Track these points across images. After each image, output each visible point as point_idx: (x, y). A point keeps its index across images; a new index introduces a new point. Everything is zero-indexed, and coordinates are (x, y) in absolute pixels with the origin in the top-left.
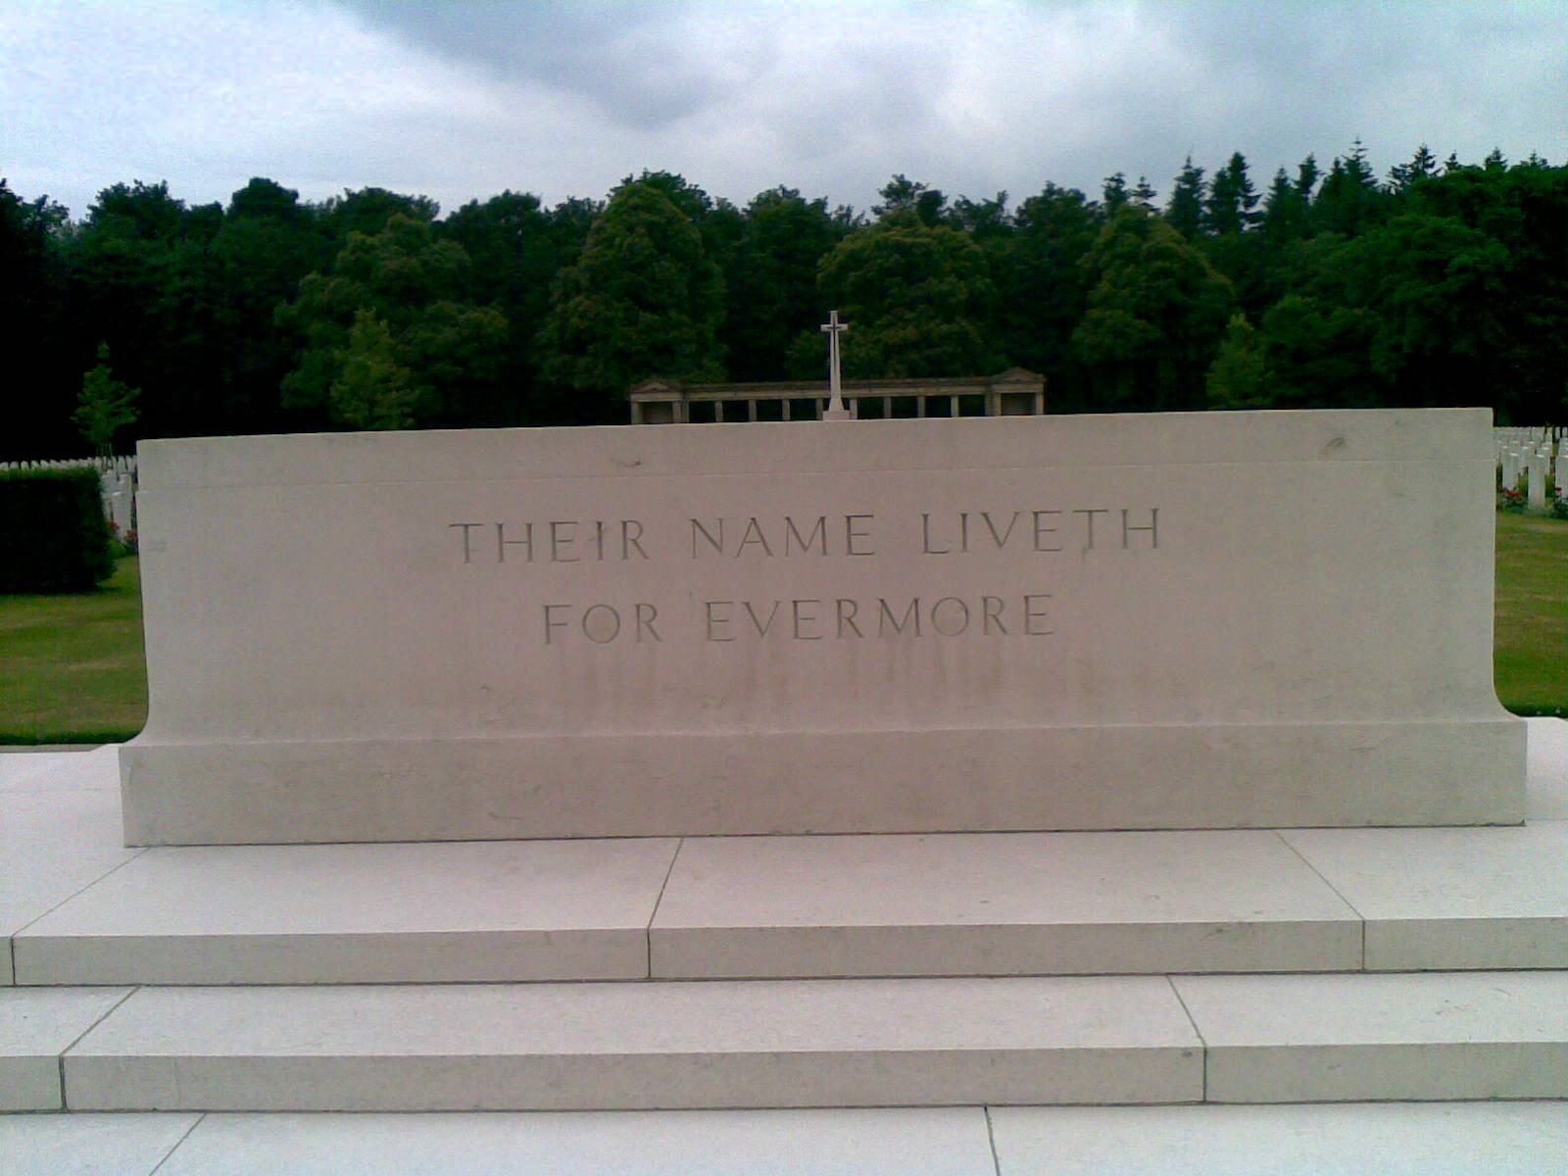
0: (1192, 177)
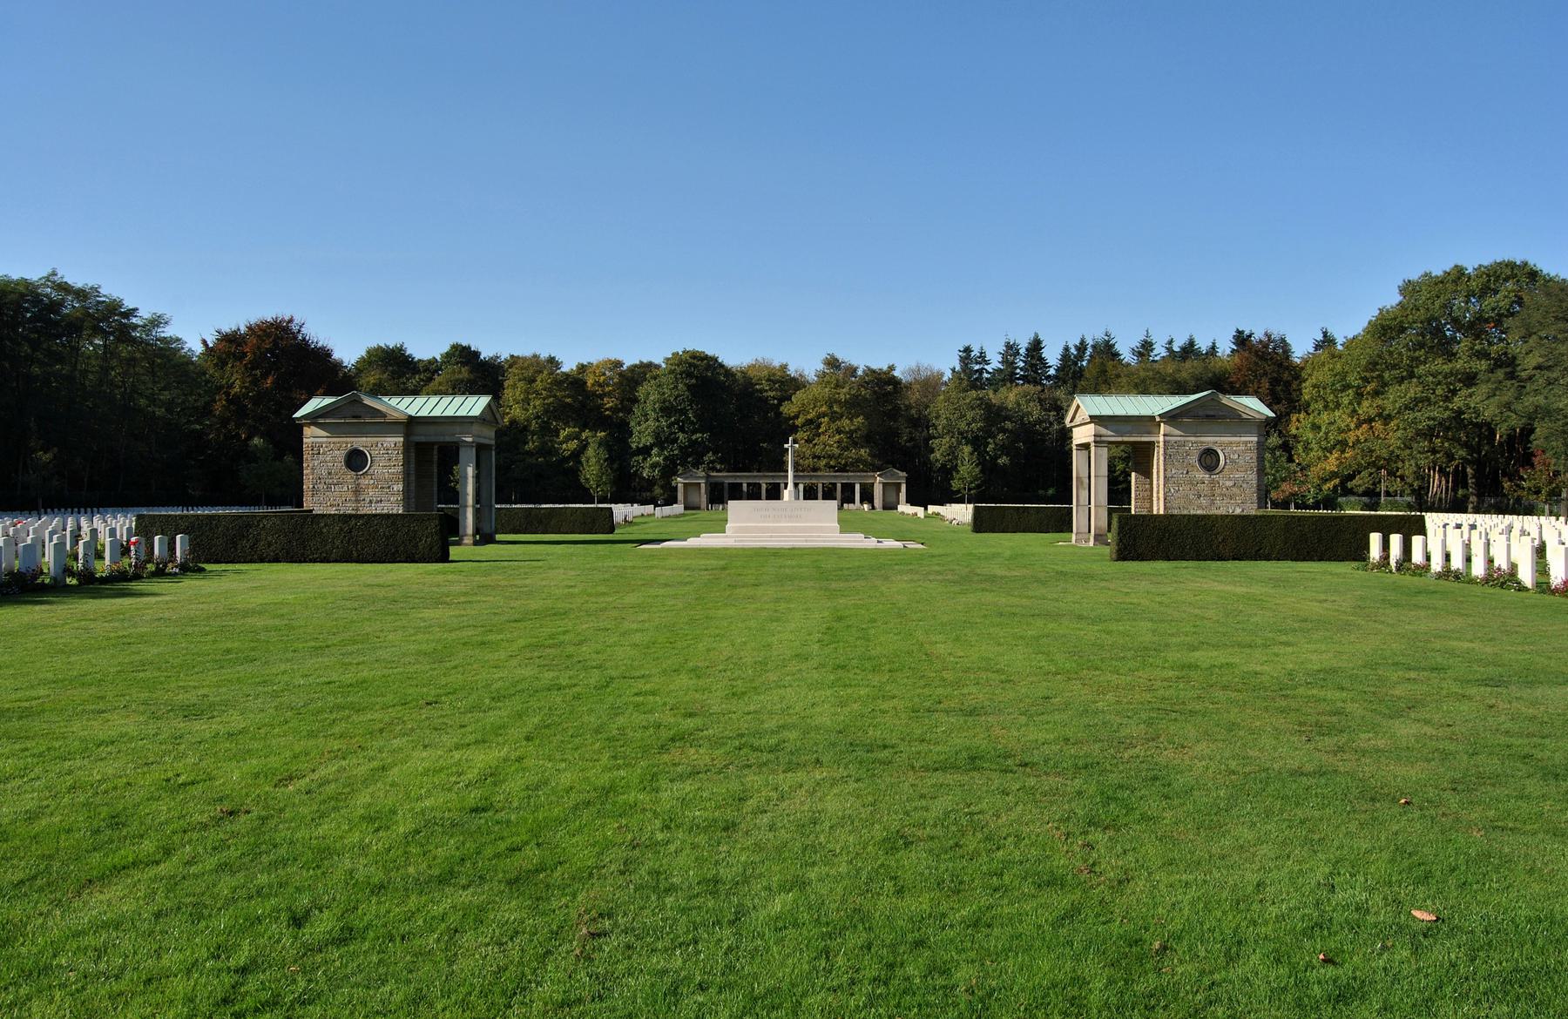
0: (1011, 349)
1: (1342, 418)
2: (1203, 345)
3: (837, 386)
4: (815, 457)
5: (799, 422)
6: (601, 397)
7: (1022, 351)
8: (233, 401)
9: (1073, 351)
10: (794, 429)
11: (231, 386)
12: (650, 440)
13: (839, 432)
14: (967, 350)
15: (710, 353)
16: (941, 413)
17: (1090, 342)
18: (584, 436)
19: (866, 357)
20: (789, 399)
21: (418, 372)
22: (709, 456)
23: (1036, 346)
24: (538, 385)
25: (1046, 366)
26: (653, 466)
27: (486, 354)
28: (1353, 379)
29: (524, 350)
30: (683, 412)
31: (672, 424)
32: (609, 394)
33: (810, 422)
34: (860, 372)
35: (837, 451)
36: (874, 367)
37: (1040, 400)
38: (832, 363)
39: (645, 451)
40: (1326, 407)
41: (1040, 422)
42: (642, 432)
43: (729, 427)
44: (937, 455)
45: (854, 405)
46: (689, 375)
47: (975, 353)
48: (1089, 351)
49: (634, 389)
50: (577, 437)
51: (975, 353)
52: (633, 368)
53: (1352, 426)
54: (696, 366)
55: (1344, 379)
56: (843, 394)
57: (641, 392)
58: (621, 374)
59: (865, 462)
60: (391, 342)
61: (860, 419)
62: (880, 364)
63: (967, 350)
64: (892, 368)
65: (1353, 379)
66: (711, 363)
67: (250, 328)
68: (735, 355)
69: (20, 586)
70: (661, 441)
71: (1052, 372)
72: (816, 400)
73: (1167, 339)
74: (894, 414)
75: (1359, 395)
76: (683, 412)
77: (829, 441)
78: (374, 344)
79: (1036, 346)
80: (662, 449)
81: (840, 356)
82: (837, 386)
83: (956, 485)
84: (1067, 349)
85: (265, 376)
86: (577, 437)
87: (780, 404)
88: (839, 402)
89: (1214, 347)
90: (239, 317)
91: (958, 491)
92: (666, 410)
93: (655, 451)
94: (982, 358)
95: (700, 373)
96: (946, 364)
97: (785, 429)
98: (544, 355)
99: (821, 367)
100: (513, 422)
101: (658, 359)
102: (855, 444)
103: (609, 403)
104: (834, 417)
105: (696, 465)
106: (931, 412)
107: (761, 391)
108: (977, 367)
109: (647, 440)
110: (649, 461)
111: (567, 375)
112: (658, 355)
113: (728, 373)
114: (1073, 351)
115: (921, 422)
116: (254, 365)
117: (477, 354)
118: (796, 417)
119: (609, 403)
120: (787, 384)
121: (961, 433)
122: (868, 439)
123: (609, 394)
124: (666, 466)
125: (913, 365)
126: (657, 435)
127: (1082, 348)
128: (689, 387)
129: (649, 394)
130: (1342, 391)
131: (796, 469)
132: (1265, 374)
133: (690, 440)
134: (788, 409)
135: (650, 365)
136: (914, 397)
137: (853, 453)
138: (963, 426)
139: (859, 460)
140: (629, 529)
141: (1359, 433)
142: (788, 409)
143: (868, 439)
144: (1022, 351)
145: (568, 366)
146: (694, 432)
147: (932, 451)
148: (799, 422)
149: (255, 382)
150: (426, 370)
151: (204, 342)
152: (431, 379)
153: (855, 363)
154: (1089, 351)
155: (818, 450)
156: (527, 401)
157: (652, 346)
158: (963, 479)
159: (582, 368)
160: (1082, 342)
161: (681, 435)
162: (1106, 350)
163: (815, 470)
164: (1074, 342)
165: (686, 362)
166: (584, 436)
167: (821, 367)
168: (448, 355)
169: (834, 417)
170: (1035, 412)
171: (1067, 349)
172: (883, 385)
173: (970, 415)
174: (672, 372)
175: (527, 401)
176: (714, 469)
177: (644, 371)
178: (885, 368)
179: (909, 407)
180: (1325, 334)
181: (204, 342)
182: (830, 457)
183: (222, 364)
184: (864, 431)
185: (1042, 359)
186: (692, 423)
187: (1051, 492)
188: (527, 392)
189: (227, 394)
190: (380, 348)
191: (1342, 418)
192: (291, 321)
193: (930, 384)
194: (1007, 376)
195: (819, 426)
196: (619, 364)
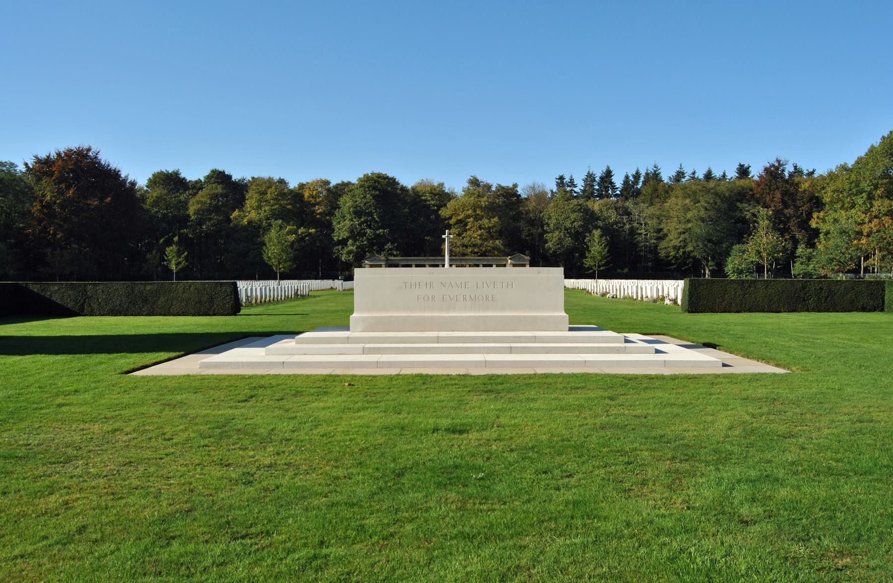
0: (590, 178)
1: (857, 214)
2: (717, 173)
3: (479, 196)
4: (463, 245)
5: (452, 221)
6: (314, 205)
7: (597, 179)
8: (48, 206)
9: (631, 178)
10: (449, 227)
11: (44, 196)
12: (346, 234)
13: (480, 228)
14: (561, 178)
15: (390, 175)
16: (552, 216)
17: (643, 173)
18: (300, 232)
19: (497, 178)
20: (445, 205)
21: (188, 189)
22: (389, 246)
23: (608, 174)
24: (269, 196)
25: (614, 188)
26: (349, 253)
27: (236, 177)
28: (865, 185)
29: (264, 173)
30: (370, 214)
31: (363, 223)
32: (319, 204)
33: (459, 222)
34: (494, 189)
35: (479, 242)
36: (504, 184)
37: (616, 209)
38: (474, 182)
39: (343, 242)
40: (842, 208)
41: (616, 223)
42: (341, 228)
43: (405, 225)
44: (550, 244)
45: (491, 209)
46: (375, 188)
47: (567, 180)
48: (642, 179)
49: (337, 200)
50: (295, 232)
51: (567, 180)
52: (337, 186)
53: (867, 220)
54: (379, 182)
55: (857, 186)
56: (484, 202)
57: (341, 201)
58: (329, 190)
59: (499, 250)
60: (169, 168)
61: (496, 219)
62: (507, 183)
63: (561, 178)
64: (515, 186)
65: (865, 185)
66: (392, 182)
67: (59, 155)
68: (408, 180)
69: (740, 247)
70: (354, 234)
71: (618, 192)
72: (464, 206)
73: (692, 171)
74: (517, 217)
75: (871, 197)
76: (370, 214)
77: (474, 235)
78: (157, 170)
79: (608, 174)
80: (355, 240)
81: (480, 178)
82: (479, 196)
83: (588, 262)
84: (627, 177)
85: (68, 188)
86: (295, 232)
87: (439, 209)
88: (481, 207)
89: (724, 176)
90: (51, 146)
91: (590, 268)
92: (358, 213)
93: (350, 242)
94: (572, 183)
95: (382, 189)
96: (550, 186)
97: (443, 225)
98: (276, 177)
99: (466, 185)
100: (250, 222)
101: (354, 181)
102: (492, 237)
103: (319, 209)
104: (477, 218)
105: (379, 252)
106: (545, 215)
107: (426, 201)
108: (568, 189)
109: (344, 234)
110: (346, 250)
111: (291, 191)
112: (353, 177)
113: (403, 189)
114: (631, 178)
115: (537, 222)
116: (60, 181)
117: (230, 177)
118: (450, 218)
119: (319, 209)
120: (442, 197)
121: (566, 229)
122: (501, 234)
123: (319, 204)
124: (357, 253)
125: (531, 184)
126: (352, 230)
127: (637, 176)
128: (374, 197)
129: (346, 202)
130: (856, 195)
131: (451, 255)
132: (778, 188)
133: (375, 234)
134: (444, 213)
135: (349, 183)
136: (531, 206)
137: (490, 243)
138: (568, 224)
139: (494, 248)
140: (272, 307)
141: (872, 225)
142: (444, 213)
143: (501, 234)
144: (597, 179)
145: (293, 184)
146: (378, 229)
147: (546, 241)
148: (452, 221)
149: (61, 193)
150: (194, 187)
151: (26, 164)
152: (195, 194)
153: (490, 182)
154: (642, 179)
155: (466, 241)
156: (259, 207)
157: (347, 171)
158: (594, 258)
159: (302, 186)
160: (637, 173)
161: (368, 231)
162: (654, 177)
163: (464, 255)
164: (632, 172)
165: (372, 179)
166: (300, 232)
167: (466, 185)
168: (208, 178)
169: (477, 218)
170: (613, 216)
171: (627, 177)
172: (509, 195)
173: (573, 216)
174: (361, 186)
175: (259, 207)
176: (392, 255)
177: (343, 188)
178: (511, 186)
179: (528, 212)
180: (795, 167)
181: (26, 164)
182: (475, 246)
183: (39, 180)
184: (498, 228)
185: (611, 183)
186: (376, 222)
187: (626, 271)
188: (260, 201)
189: (41, 201)
190: (161, 173)
191: (857, 214)
192: (89, 150)
193: (540, 197)
194: (588, 194)
195: (466, 225)
196: (328, 183)
